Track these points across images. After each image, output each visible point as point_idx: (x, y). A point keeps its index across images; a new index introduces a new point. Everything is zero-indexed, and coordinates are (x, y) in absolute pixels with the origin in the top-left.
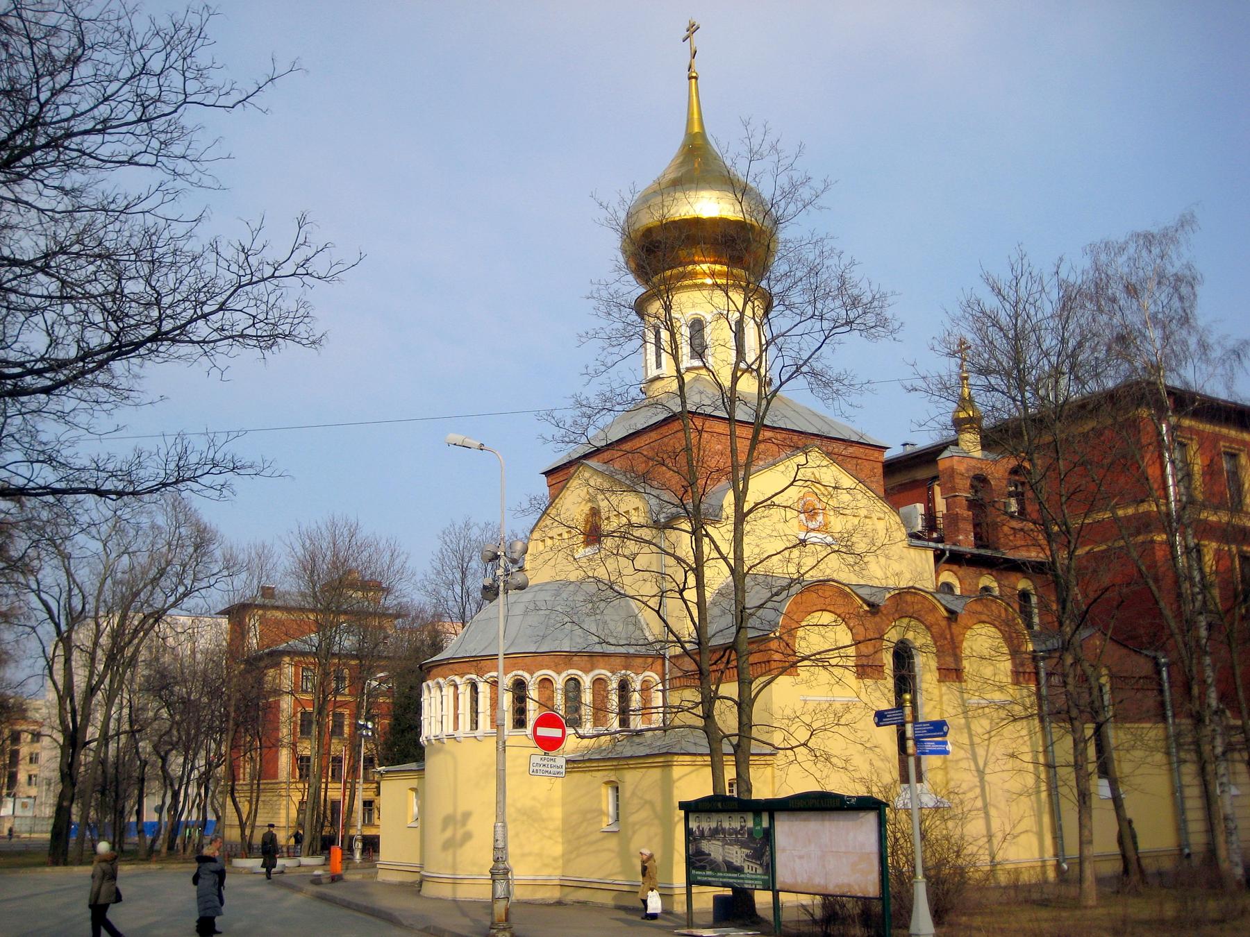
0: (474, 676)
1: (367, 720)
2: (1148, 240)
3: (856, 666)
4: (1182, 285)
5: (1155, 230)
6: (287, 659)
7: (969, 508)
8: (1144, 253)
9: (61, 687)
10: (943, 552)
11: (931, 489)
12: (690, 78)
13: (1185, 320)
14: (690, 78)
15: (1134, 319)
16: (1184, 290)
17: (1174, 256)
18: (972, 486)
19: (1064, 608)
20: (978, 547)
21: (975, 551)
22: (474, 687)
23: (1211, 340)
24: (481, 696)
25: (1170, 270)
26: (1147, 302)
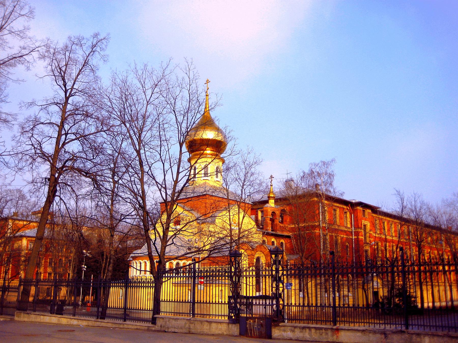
2: (324, 163)
3: (316, 277)
4: (331, 176)
5: (326, 161)
9: (159, 251)
10: (265, 232)
12: (206, 96)
13: (331, 184)
14: (206, 96)
17: (330, 168)
18: (272, 215)
20: (272, 231)
21: (272, 232)
26: (322, 178)
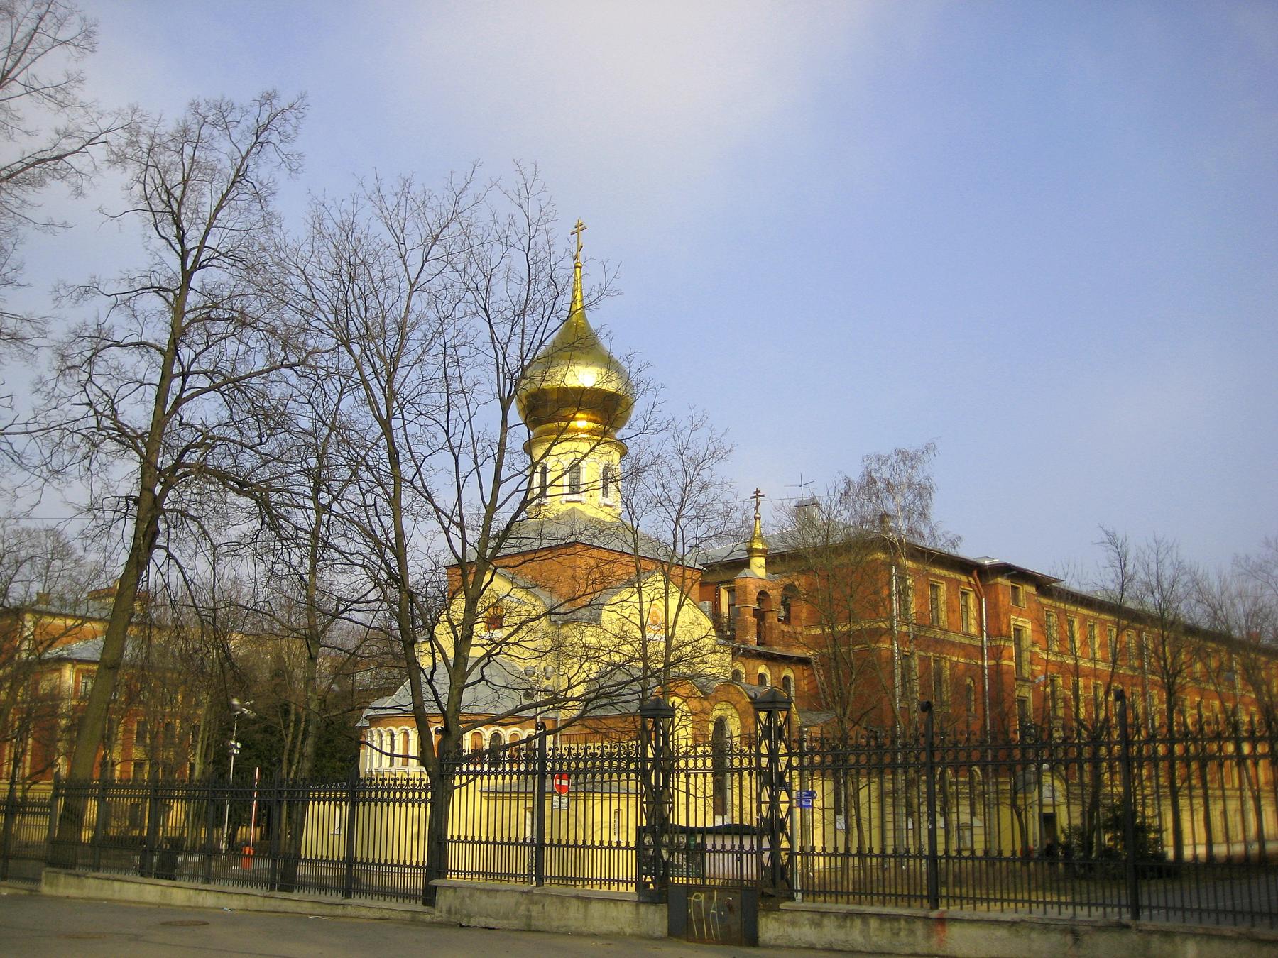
0: (407, 728)
1: (236, 742)
2: (904, 456)
4: (923, 491)
6: (69, 666)
7: (754, 616)
8: (901, 464)
11: (717, 591)
12: (576, 267)
13: (923, 515)
15: (890, 506)
16: (925, 495)
19: (844, 714)
22: (392, 735)
23: (937, 533)
24: (411, 743)
25: (916, 480)
26: (899, 498)
